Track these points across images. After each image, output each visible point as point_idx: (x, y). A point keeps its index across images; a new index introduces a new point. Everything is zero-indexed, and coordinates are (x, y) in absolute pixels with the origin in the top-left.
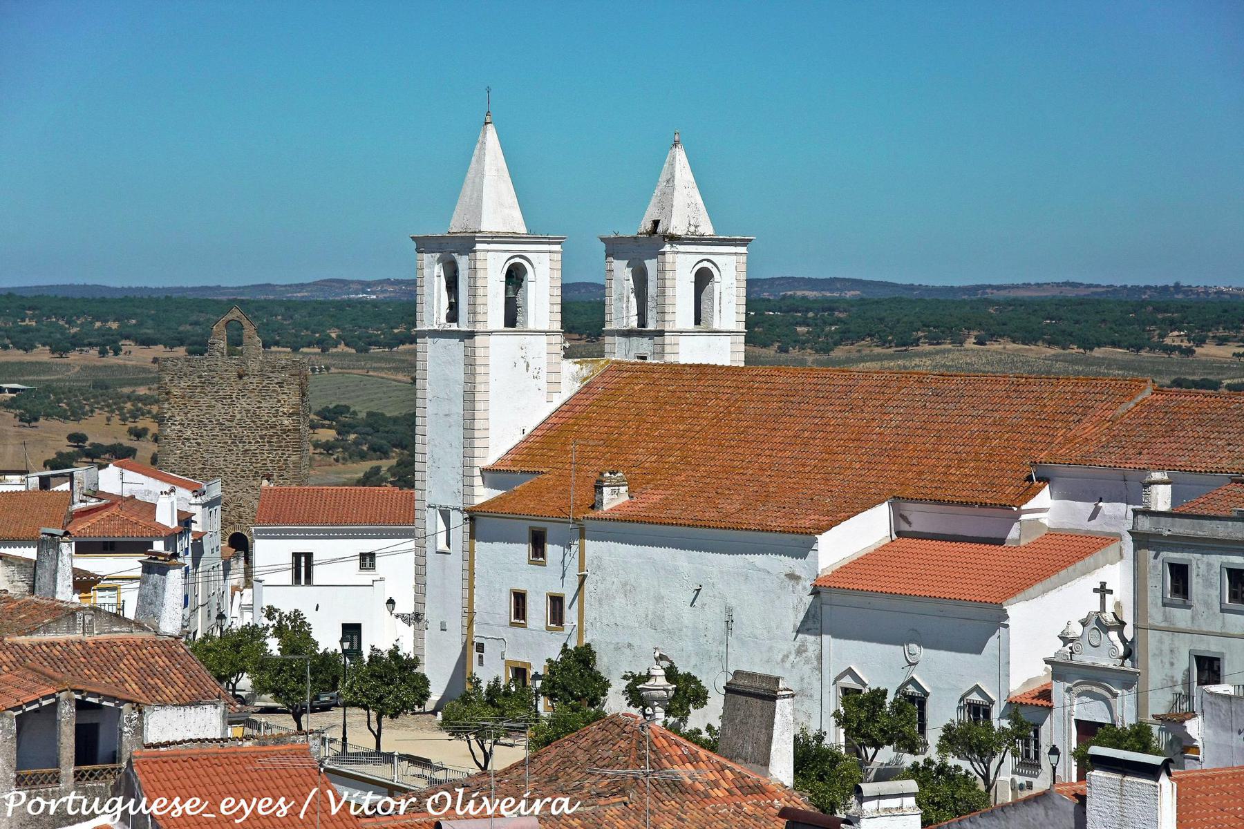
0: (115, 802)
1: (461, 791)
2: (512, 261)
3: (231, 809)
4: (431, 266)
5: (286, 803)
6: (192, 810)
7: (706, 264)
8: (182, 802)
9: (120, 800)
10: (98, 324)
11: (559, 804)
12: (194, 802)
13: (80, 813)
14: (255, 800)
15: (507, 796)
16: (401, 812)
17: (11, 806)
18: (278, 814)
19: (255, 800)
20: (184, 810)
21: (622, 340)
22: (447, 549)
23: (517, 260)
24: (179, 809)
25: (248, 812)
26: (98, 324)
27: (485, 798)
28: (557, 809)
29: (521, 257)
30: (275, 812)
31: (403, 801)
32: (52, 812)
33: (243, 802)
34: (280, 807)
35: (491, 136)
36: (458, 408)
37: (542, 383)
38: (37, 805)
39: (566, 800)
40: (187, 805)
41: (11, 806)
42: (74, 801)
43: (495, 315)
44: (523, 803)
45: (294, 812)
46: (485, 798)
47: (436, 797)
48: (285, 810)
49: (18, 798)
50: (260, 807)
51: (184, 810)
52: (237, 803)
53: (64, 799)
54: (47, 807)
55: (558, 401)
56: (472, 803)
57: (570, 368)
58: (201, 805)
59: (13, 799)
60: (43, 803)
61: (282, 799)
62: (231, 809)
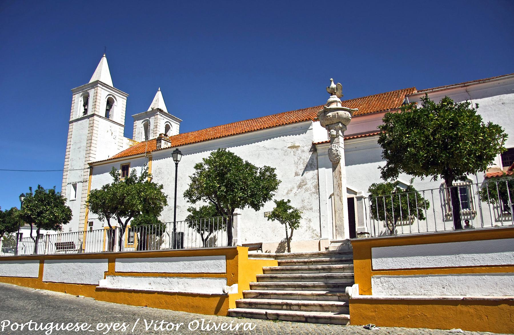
0: (50, 325)
3: (86, 328)
4: (78, 98)
5: (126, 326)
7: (168, 123)
8: (79, 325)
9: (52, 324)
10: (141, 213)
12: (70, 325)
15: (83, 322)
16: (177, 329)
17: (3, 326)
22: (74, 199)
23: (111, 96)
24: (78, 328)
25: (109, 329)
26: (141, 213)
28: (246, 328)
29: (113, 96)
31: (22, 324)
32: (22, 329)
33: (107, 325)
34: (76, 327)
35: (104, 61)
36: (84, 144)
38: (14, 327)
40: (82, 326)
41: (3, 326)
47: (192, 323)
48: (125, 328)
49: (6, 323)
50: (114, 327)
53: (27, 324)
56: (208, 325)
58: (88, 326)
59: (4, 323)
62: (86, 328)
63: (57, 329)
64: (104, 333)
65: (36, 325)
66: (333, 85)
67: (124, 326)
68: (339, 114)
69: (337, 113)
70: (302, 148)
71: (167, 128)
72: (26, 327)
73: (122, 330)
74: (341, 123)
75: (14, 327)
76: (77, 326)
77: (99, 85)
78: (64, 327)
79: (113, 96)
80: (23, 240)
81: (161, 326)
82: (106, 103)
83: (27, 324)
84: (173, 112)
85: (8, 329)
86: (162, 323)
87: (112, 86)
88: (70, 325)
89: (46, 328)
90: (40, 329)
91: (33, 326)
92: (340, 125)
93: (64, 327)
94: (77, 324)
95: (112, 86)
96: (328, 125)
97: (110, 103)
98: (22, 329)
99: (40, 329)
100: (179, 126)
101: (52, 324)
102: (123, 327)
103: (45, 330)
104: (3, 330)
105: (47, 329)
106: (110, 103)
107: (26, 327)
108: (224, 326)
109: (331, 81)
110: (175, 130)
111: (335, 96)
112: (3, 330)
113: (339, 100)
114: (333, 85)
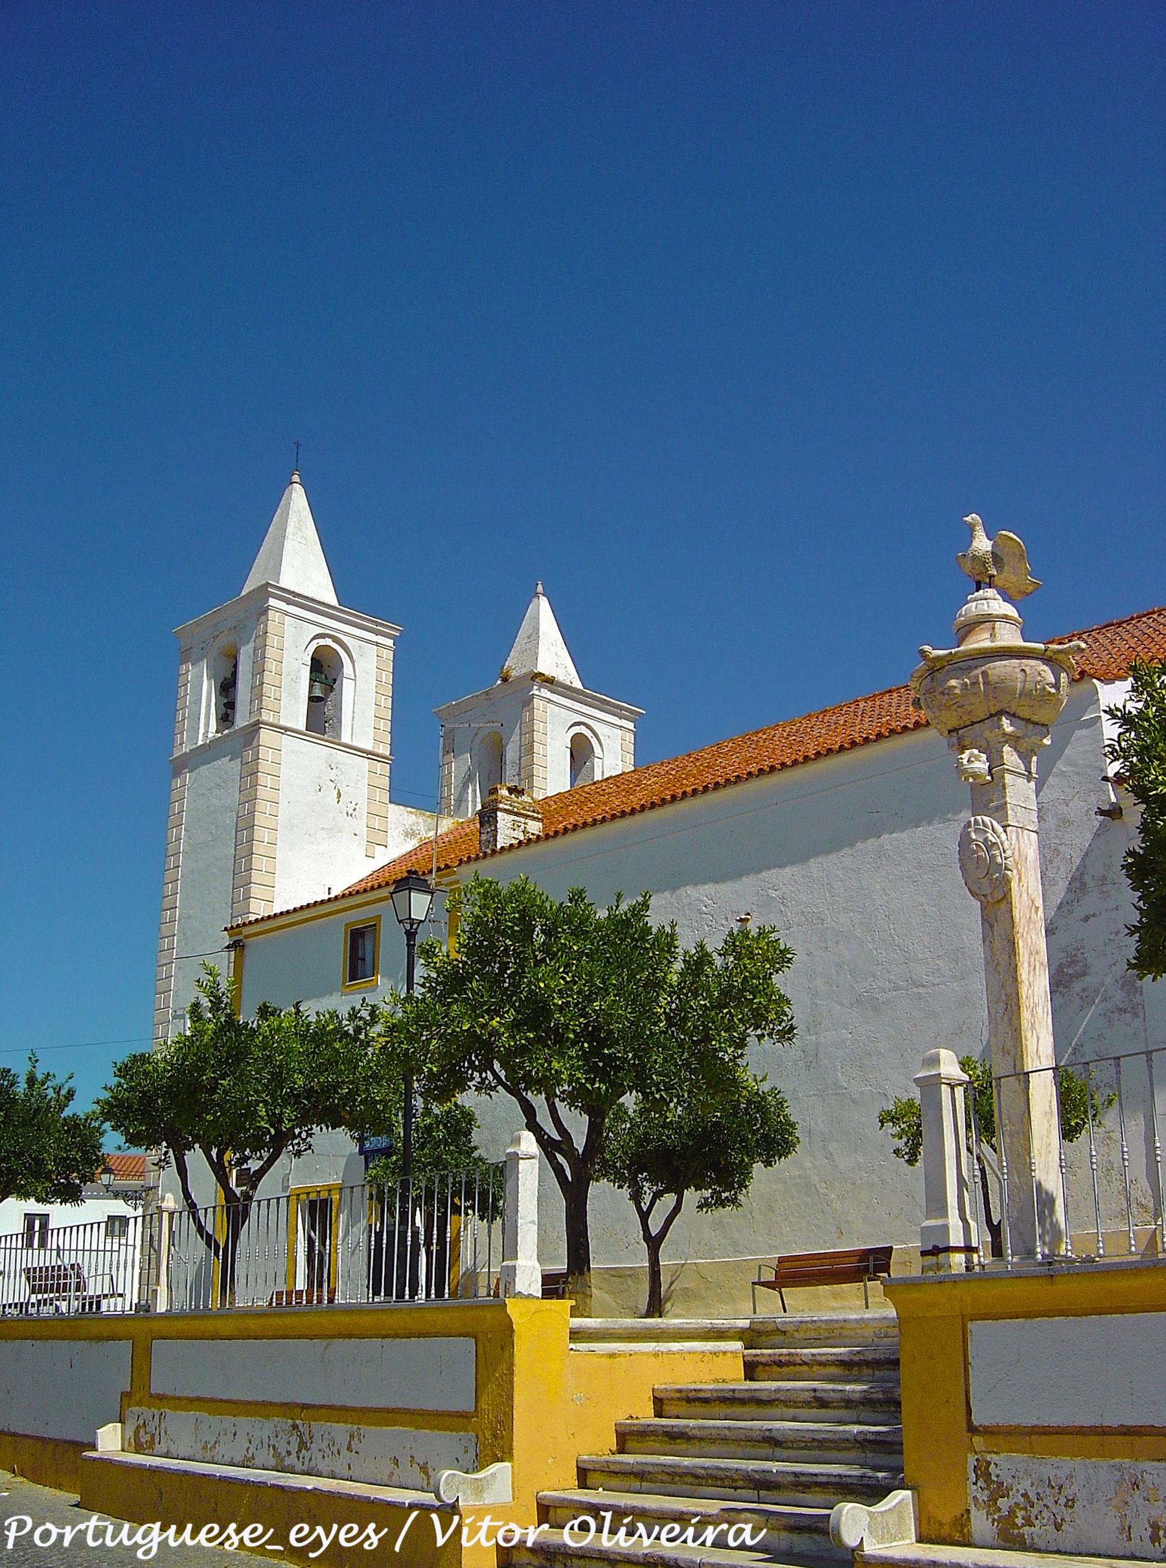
1: (608, 1515)
2: (322, 642)
5: (376, 1532)
6: (252, 1540)
7: (582, 729)
8: (238, 1531)
11: (740, 1532)
13: (103, 1544)
14: (335, 1527)
17: (12, 1534)
18: (366, 1546)
19: (335, 1527)
20: (241, 1540)
21: (1138, 1554)
24: (235, 1539)
25: (326, 1543)
27: (640, 1525)
29: (336, 640)
30: (222, 1544)
31: (68, 1528)
32: (66, 1543)
33: (320, 1530)
34: (368, 1537)
37: (360, 825)
38: (46, 1535)
39: (748, 1528)
40: (246, 1534)
42: (489, 1527)
43: (295, 713)
44: (690, 1532)
45: (386, 1543)
46: (640, 1525)
48: (375, 1539)
49: (21, 1525)
50: (664, 1536)
51: (241, 1540)
52: (312, 1531)
53: (82, 1526)
54: (61, 1537)
55: (383, 857)
56: (623, 1530)
57: (401, 817)
59: (14, 1525)
60: (55, 1531)
61: (372, 1526)
63: (172, 1543)
64: (312, 1555)
65: (110, 1529)
66: (982, 544)
67: (372, 1534)
68: (993, 678)
69: (984, 673)
70: (1062, 809)
71: (581, 752)
72: (80, 1537)
73: (227, 1545)
74: (1012, 716)
75: (46, 1535)
76: (233, 1534)
77: (272, 602)
78: (194, 1534)
79: (336, 640)
80: (52, 1242)
81: (482, 1535)
82: (306, 672)
83: (82, 1526)
84: (601, 680)
85: (24, 1542)
86: (486, 1523)
87: (335, 603)
88: (211, 1530)
89: (138, 1538)
90: (184, 1542)
91: (99, 1533)
92: (1007, 726)
93: (194, 1534)
94: (233, 1526)
95: (335, 603)
96: (955, 730)
97: (324, 670)
98: (66, 1543)
99: (184, 1542)
100: (630, 737)
101: (157, 1526)
102: (228, 1538)
103: (137, 1546)
104: (10, 1546)
105: (141, 1542)
106: (324, 670)
107: (80, 1537)
108: (348, 1532)
109: (971, 528)
110: (614, 755)
111: (991, 592)
112: (10, 1546)
113: (1010, 610)
114: (982, 544)
